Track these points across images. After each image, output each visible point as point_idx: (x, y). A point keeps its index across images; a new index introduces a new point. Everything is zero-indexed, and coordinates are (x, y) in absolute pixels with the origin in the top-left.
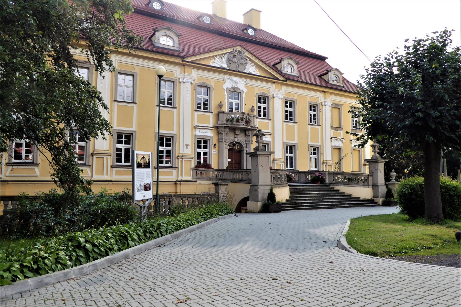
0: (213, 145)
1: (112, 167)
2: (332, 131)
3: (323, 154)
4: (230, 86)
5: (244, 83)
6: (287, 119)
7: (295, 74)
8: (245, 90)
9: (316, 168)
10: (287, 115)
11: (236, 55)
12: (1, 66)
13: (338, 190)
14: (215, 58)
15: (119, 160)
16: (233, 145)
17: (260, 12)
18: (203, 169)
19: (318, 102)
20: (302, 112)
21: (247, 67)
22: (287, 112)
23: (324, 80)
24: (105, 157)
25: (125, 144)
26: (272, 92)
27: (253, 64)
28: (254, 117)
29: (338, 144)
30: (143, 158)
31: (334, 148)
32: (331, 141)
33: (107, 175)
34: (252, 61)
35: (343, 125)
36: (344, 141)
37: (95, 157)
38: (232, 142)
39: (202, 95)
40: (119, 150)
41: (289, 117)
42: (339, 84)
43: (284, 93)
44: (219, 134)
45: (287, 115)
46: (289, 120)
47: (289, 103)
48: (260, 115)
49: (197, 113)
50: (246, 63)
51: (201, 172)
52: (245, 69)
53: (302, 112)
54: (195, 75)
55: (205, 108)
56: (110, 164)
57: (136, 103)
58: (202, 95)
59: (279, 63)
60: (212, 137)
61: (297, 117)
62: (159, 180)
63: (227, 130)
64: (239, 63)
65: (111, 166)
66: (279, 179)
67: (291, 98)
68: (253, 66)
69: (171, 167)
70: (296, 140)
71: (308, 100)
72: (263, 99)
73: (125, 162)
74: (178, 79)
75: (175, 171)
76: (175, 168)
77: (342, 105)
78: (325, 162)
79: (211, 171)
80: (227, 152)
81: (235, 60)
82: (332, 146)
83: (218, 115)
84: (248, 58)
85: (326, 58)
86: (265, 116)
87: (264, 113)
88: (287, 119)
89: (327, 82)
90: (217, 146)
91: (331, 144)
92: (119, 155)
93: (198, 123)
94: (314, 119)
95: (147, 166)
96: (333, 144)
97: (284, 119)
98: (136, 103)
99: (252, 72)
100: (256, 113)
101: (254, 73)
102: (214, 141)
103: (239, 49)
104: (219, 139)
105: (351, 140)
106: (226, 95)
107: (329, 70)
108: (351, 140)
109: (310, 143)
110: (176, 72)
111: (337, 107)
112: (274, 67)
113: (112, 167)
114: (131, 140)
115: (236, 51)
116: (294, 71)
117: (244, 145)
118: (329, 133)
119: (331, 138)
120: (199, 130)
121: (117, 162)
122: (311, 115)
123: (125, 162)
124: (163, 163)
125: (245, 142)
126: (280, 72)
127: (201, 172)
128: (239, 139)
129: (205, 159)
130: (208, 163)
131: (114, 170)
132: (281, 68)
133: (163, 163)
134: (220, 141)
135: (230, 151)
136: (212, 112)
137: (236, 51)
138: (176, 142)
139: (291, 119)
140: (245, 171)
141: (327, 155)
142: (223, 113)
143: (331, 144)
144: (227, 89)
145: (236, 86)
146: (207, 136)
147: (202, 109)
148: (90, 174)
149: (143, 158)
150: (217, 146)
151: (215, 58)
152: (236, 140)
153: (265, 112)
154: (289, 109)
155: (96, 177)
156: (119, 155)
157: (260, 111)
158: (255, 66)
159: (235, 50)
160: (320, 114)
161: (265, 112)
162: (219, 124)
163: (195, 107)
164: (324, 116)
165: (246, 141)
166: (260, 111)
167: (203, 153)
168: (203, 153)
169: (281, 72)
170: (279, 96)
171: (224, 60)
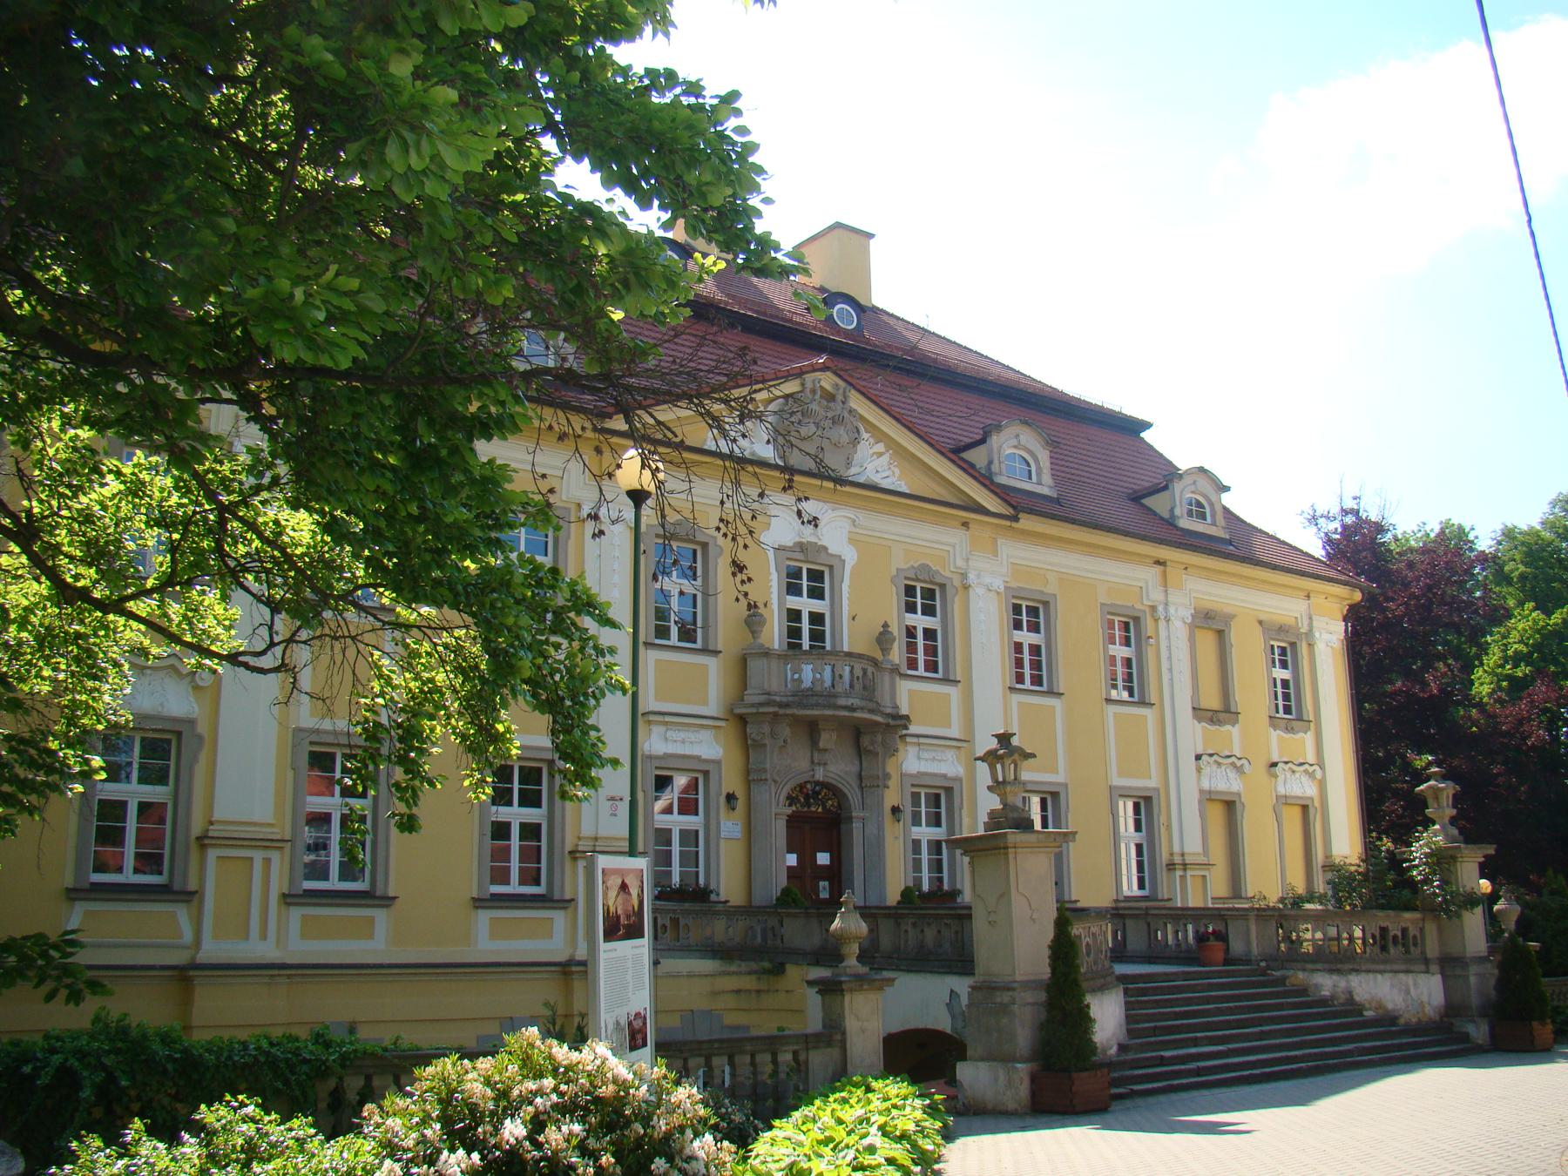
0: (723, 799)
1: (289, 899)
2: (1199, 727)
3: (1169, 827)
4: (788, 540)
5: (847, 526)
6: (1020, 678)
7: (1045, 491)
8: (850, 556)
9: (1141, 886)
10: (1019, 663)
11: (814, 406)
12: (3, 360)
13: (1303, 991)
16: (807, 797)
17: (870, 236)
18: (687, 905)
19: (1138, 606)
20: (1080, 649)
21: (858, 456)
22: (1018, 647)
23: (1155, 513)
24: (258, 856)
25: (141, 781)
26: (960, 563)
27: (880, 447)
28: (895, 670)
29: (1224, 781)
30: (624, 887)
31: (1208, 797)
32: (1199, 770)
34: (880, 436)
36: (1247, 768)
37: (212, 854)
38: (802, 787)
41: (1032, 671)
42: (1212, 531)
44: (748, 745)
45: (1019, 663)
46: (1027, 685)
47: (1028, 613)
48: (912, 664)
50: (855, 441)
51: (675, 922)
52: (849, 465)
56: (278, 884)
59: (982, 441)
60: (718, 763)
63: (785, 731)
64: (825, 444)
65: (285, 896)
66: (1088, 954)
68: (880, 455)
70: (1061, 769)
72: (924, 594)
74: (573, 507)
75: (559, 918)
76: (566, 904)
78: (1177, 859)
79: (718, 913)
80: (781, 827)
82: (1202, 792)
83: (743, 661)
84: (862, 418)
85: (1146, 425)
86: (932, 666)
87: (932, 656)
88: (1020, 678)
89: (1170, 523)
90: (740, 804)
91: (1199, 779)
93: (657, 699)
94: (1133, 681)
95: (634, 932)
96: (1206, 785)
97: (1010, 679)
100: (897, 654)
101: (885, 484)
102: (731, 780)
103: (827, 381)
104: (748, 772)
105: (1274, 765)
106: (774, 576)
107: (1167, 475)
108: (1274, 765)
109: (1118, 781)
111: (1213, 624)
112: (955, 453)
113: (289, 899)
114: (172, 763)
115: (813, 391)
116: (1039, 474)
117: (853, 796)
118: (1191, 734)
119: (1198, 757)
120: (662, 729)
125: (855, 784)
126: (986, 480)
127: (675, 922)
128: (832, 768)
129: (690, 859)
130: (702, 881)
131: (296, 914)
132: (990, 462)
133: (507, 882)
134: (751, 777)
135: (792, 821)
136: (716, 653)
138: (195, 759)
139: (1037, 680)
140: (888, 916)
141: (1188, 832)
142: (766, 653)
143: (1199, 779)
145: (813, 539)
146: (698, 758)
148: (188, 936)
149: (624, 887)
150: (740, 804)
152: (820, 775)
153: (931, 651)
154: (1026, 638)
155: (213, 949)
157: (912, 648)
158: (885, 459)
159: (809, 385)
160: (1150, 654)
161: (931, 651)
162: (753, 705)
164: (1165, 665)
165: (860, 777)
166: (912, 648)
169: (992, 482)
170: (987, 580)
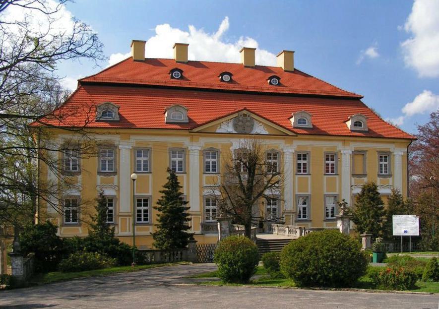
14: (222, 124)
15: (68, 220)
27: (261, 124)
33: (129, 231)
35: (368, 171)
39: (302, 161)
40: (139, 211)
41: (301, 169)
43: (296, 147)
49: (205, 175)
53: (317, 164)
54: (204, 142)
55: (214, 170)
57: (366, 175)
58: (302, 161)
61: (311, 169)
62: (135, 235)
64: (245, 126)
67: (303, 150)
69: (148, 224)
70: (309, 191)
71: (325, 150)
73: (144, 221)
77: (367, 151)
81: (240, 123)
92: (139, 215)
98: (366, 175)
99: (259, 132)
110: (184, 141)
115: (241, 115)
121: (138, 221)
122: (381, 165)
123: (144, 221)
124: (141, 221)
137: (241, 115)
144: (235, 150)
147: (211, 172)
151: (222, 124)
156: (139, 215)
163: (203, 169)
167: (144, 210)
168: (144, 210)
171: (231, 124)
